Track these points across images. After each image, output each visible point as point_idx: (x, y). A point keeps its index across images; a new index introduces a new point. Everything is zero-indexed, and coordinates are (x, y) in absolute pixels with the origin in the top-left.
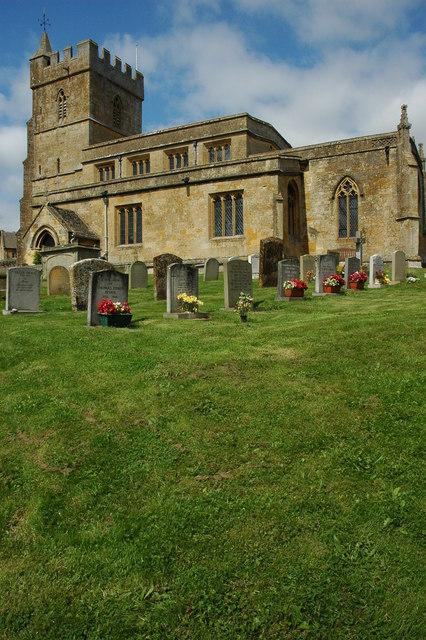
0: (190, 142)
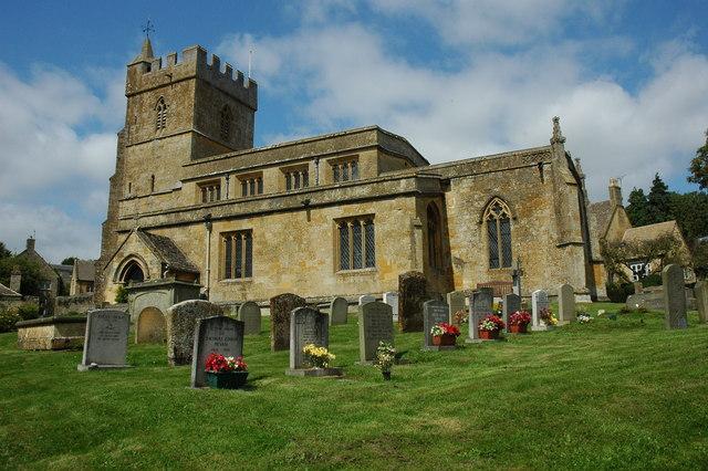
0: (312, 158)
